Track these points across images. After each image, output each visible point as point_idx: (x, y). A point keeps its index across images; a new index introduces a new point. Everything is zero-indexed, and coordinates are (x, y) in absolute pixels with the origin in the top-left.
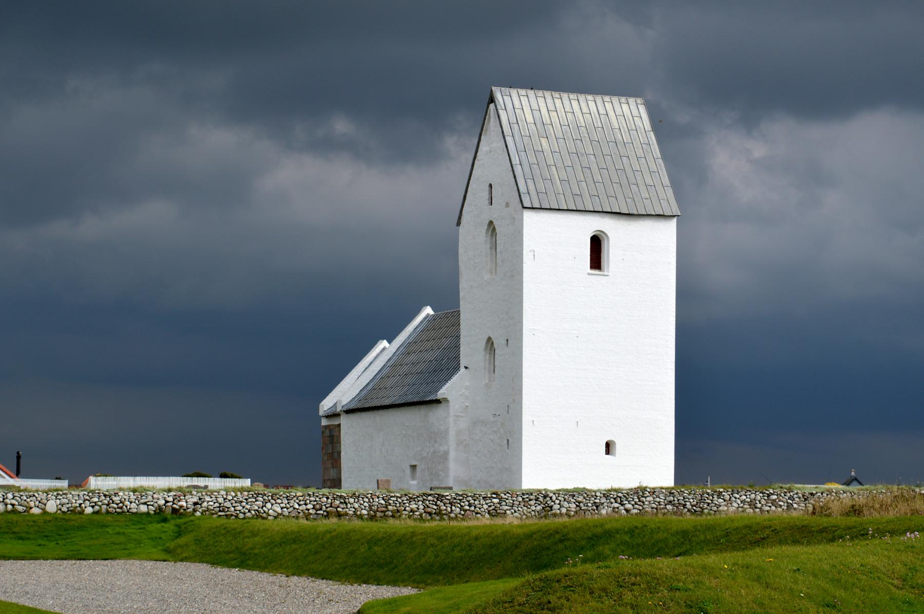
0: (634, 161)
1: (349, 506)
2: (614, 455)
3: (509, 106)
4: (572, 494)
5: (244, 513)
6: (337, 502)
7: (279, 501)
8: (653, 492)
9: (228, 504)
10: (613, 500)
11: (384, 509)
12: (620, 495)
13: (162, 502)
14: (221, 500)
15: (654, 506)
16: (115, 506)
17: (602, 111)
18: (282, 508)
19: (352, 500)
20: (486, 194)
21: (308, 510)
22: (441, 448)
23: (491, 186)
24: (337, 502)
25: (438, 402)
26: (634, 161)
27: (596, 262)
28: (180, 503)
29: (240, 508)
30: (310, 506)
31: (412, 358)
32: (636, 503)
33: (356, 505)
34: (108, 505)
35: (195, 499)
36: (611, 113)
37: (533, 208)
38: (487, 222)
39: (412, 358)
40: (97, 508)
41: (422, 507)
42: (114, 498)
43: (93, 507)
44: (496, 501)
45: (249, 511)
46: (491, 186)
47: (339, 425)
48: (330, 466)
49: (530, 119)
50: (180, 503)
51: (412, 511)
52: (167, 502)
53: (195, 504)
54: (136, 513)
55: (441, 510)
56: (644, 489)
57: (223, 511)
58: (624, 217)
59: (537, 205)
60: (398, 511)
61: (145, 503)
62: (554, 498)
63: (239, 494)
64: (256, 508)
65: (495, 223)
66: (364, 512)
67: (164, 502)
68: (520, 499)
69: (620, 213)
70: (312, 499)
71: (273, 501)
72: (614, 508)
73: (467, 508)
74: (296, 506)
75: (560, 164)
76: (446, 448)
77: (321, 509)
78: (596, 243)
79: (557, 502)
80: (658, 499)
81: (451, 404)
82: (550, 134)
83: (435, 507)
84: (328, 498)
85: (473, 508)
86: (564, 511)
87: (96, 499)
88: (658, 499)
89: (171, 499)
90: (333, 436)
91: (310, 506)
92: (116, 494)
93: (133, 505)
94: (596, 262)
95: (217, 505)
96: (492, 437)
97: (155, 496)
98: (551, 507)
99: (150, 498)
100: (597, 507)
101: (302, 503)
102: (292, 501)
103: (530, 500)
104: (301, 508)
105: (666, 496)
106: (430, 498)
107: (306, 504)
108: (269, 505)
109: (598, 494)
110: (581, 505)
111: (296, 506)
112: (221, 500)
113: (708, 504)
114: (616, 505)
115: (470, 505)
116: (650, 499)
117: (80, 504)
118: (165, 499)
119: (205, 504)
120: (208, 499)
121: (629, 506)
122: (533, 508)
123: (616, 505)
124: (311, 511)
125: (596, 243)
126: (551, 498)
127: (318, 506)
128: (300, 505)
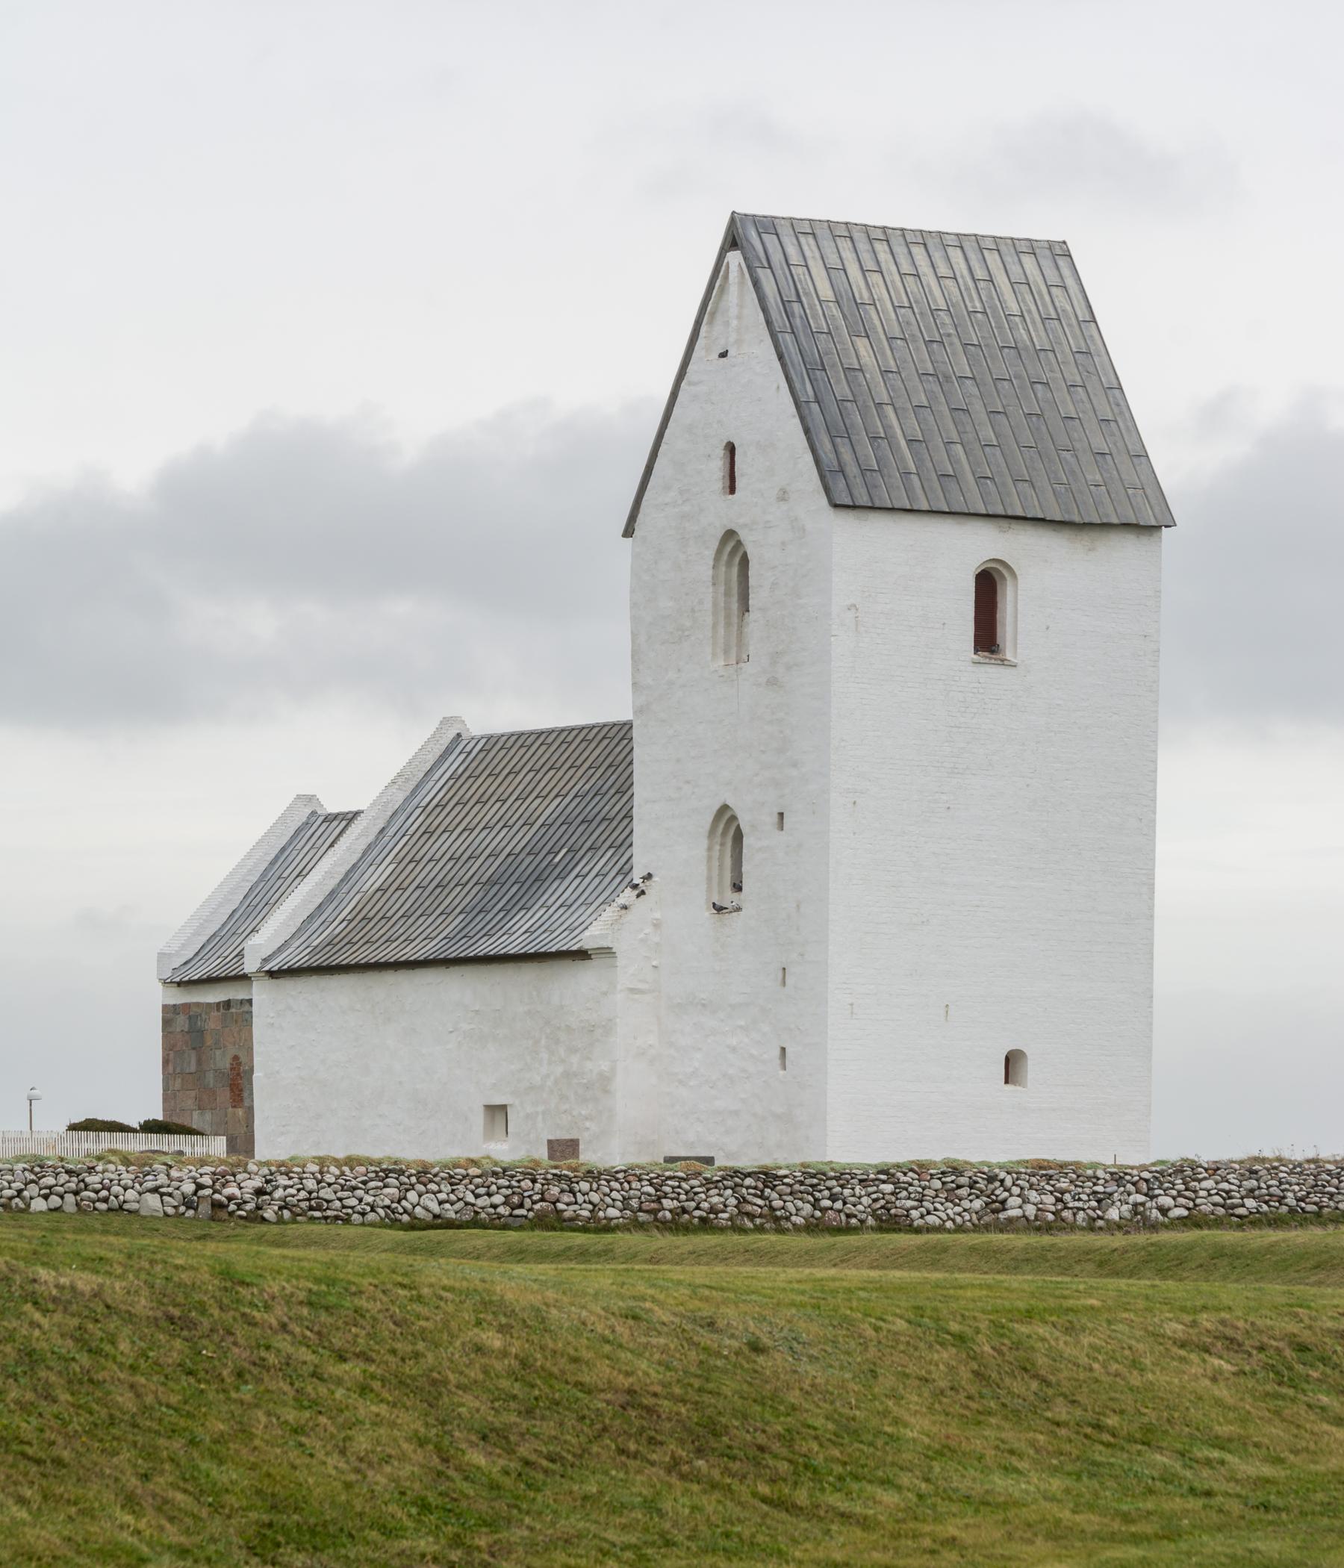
0: (1061, 395)
1: (580, 1198)
2: (1014, 1083)
3: (777, 257)
4: (1043, 1171)
5: (363, 1214)
6: (555, 1190)
7: (433, 1187)
8: (1214, 1170)
9: (326, 1193)
10: (1132, 1188)
11: (654, 1205)
12: (1146, 1175)
13: (188, 1188)
14: (311, 1184)
15: (1217, 1199)
16: (92, 1195)
17: (980, 273)
18: (440, 1203)
19: (584, 1186)
20: (717, 466)
21: (494, 1206)
22: (589, 1065)
23: (731, 449)
24: (555, 1190)
25: (582, 955)
26: (1061, 395)
27: (987, 637)
28: (228, 1191)
29: (353, 1202)
30: (498, 1199)
31: (443, 844)
32: (1180, 1194)
33: (595, 1197)
34: (76, 1193)
35: (258, 1182)
36: (1001, 279)
37: (854, 507)
38: (720, 533)
39: (443, 844)
40: (54, 1201)
41: (733, 1201)
42: (565, 1187)
43: (46, 1197)
44: (888, 1188)
45: (373, 1210)
46: (731, 449)
47: (250, 1002)
48: (190, 1103)
49: (826, 292)
50: (228, 1191)
51: (713, 1210)
52: (200, 1187)
53: (259, 1192)
54: (135, 1212)
55: (772, 1209)
56: (1194, 1166)
57: (319, 1208)
58: (962, 519)
59: (864, 500)
60: (684, 1211)
61: (155, 1190)
62: (1008, 1182)
63: (346, 1169)
64: (387, 1202)
65: (744, 535)
66: (613, 1212)
67: (193, 1187)
68: (937, 1184)
69: (1043, 520)
70: (501, 1182)
71: (420, 1188)
72: (1135, 1205)
73: (826, 1203)
74: (470, 1198)
75: (902, 402)
76: (605, 1066)
77: (521, 1206)
78: (988, 586)
79: (1016, 1190)
80: (1225, 1186)
81: (621, 962)
82: (875, 328)
83: (760, 1202)
84: (534, 1181)
85: (839, 1205)
86: (1030, 1210)
87: (50, 1181)
88: (1225, 1186)
89: (206, 1180)
90: (201, 1032)
91: (498, 1199)
92: (91, 1170)
93: (131, 1194)
94: (987, 637)
95: (303, 1194)
96: (734, 1042)
97: (174, 1173)
98: (1003, 1202)
99: (162, 1179)
100: (1099, 1201)
101: (481, 1191)
102: (461, 1187)
103: (959, 1187)
104: (480, 1202)
105: (1242, 1178)
106: (748, 1181)
107: (489, 1195)
108: (412, 1196)
109: (1100, 1173)
110: (1067, 1197)
111: (470, 1198)
112: (311, 1184)
113: (1331, 1195)
114: (1140, 1198)
115: (833, 1198)
116: (1209, 1184)
117: (20, 1192)
118: (194, 1180)
119: (279, 1193)
120: (283, 1181)
121: (1166, 1201)
122: (966, 1204)
123: (1140, 1198)
124: (501, 1210)
125: (988, 586)
126: (1002, 1181)
127: (516, 1199)
128: (477, 1196)
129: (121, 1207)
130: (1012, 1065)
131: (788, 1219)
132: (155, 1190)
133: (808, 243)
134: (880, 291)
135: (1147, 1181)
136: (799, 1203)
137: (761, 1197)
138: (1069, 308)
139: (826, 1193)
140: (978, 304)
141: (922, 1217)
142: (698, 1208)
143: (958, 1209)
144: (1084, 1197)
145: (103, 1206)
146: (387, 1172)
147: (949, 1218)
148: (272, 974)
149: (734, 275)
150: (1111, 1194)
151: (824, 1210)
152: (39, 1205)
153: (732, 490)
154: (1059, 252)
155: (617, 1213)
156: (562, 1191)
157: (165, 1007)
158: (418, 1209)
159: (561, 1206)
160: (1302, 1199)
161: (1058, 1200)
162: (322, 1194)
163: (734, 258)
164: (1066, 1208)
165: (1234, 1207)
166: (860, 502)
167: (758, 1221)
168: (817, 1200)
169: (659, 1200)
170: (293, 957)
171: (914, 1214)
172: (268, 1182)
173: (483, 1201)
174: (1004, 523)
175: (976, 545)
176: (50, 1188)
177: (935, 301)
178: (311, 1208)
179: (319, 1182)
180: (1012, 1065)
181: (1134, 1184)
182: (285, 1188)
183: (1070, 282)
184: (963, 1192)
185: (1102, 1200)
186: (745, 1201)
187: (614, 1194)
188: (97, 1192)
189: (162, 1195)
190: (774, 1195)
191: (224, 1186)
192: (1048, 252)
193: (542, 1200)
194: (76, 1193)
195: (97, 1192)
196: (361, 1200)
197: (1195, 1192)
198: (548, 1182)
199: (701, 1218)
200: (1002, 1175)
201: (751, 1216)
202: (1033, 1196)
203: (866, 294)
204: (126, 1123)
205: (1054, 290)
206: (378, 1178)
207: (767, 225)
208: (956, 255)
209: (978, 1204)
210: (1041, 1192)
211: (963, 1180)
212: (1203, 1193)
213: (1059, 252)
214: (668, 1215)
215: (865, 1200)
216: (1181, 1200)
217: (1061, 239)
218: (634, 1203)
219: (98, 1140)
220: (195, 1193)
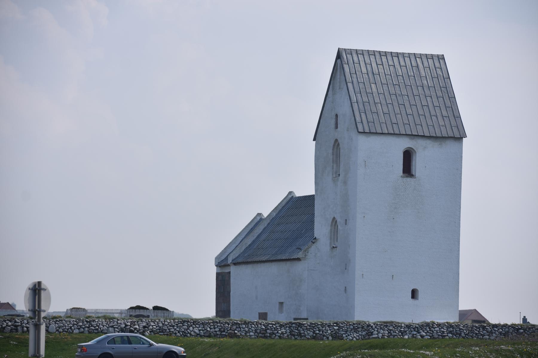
1: (242, 329)
4: (386, 325)
7: (197, 326)
8: (439, 325)
10: (412, 329)
12: (417, 326)
14: (161, 325)
18: (200, 330)
21: (216, 332)
30: (217, 329)
33: (247, 329)
34: (88, 328)
35: (144, 324)
43: (79, 329)
52: (126, 325)
53: (144, 327)
60: (273, 333)
61: (112, 327)
62: (374, 327)
64: (183, 330)
65: (339, 141)
74: (209, 329)
77: (224, 331)
78: (408, 156)
83: (297, 331)
84: (228, 324)
89: (129, 324)
91: (217, 329)
95: (158, 328)
97: (119, 322)
100: (402, 333)
101: (212, 327)
103: (358, 328)
105: (448, 328)
106: (294, 325)
107: (215, 328)
108: (191, 328)
109: (403, 325)
110: (392, 332)
111: (209, 329)
112: (161, 325)
114: (415, 333)
115: (319, 331)
118: (125, 324)
120: (152, 324)
123: (415, 333)
124: (218, 333)
125: (408, 156)
128: (211, 329)
129: (101, 332)
130: (414, 294)
131: (305, 336)
132: (112, 327)
133: (361, 57)
134: (381, 70)
135: (417, 328)
136: (309, 332)
137: (297, 330)
138: (441, 74)
139: (317, 329)
140: (412, 73)
141: (346, 336)
142: (278, 333)
143: (357, 335)
144: (397, 332)
145: (96, 331)
146: (184, 321)
147: (354, 337)
148: (235, 264)
149: (339, 66)
150: (406, 331)
151: (316, 334)
152: (76, 331)
153: (337, 127)
154: (441, 58)
155: (253, 334)
156: (237, 327)
157: (217, 273)
158: (192, 332)
159: (236, 332)
160: (467, 335)
161: (389, 332)
162: (164, 328)
163: (339, 61)
164: (391, 335)
165: (445, 336)
166: (378, 132)
167: (296, 337)
168: (314, 331)
169: (266, 330)
170: (240, 260)
171: (344, 335)
172: (147, 324)
173: (213, 330)
174: (412, 137)
175: (405, 143)
176: (80, 326)
177: (399, 73)
178: (160, 332)
179: (163, 324)
180: (414, 294)
181: (414, 328)
182: (152, 326)
183: (443, 66)
184: (360, 329)
185: (403, 333)
186: (292, 331)
187: (253, 328)
188: (95, 327)
189: (114, 328)
190: (301, 329)
191: (134, 325)
192: (437, 58)
193: (230, 330)
194: (88, 328)
195: (95, 327)
196: (175, 330)
197: (433, 331)
198: (233, 325)
199: (279, 336)
200: (372, 325)
201: (294, 335)
202: (382, 331)
203: (377, 71)
204: (145, 306)
205: (437, 69)
206: (181, 323)
207: (350, 52)
208: (407, 59)
209: (364, 333)
210: (384, 330)
211: (359, 326)
212: (435, 332)
213: (441, 58)
214: (268, 335)
215: (329, 332)
216: (428, 334)
217: (440, 53)
218: (258, 331)
219: (135, 312)
220: (125, 327)
